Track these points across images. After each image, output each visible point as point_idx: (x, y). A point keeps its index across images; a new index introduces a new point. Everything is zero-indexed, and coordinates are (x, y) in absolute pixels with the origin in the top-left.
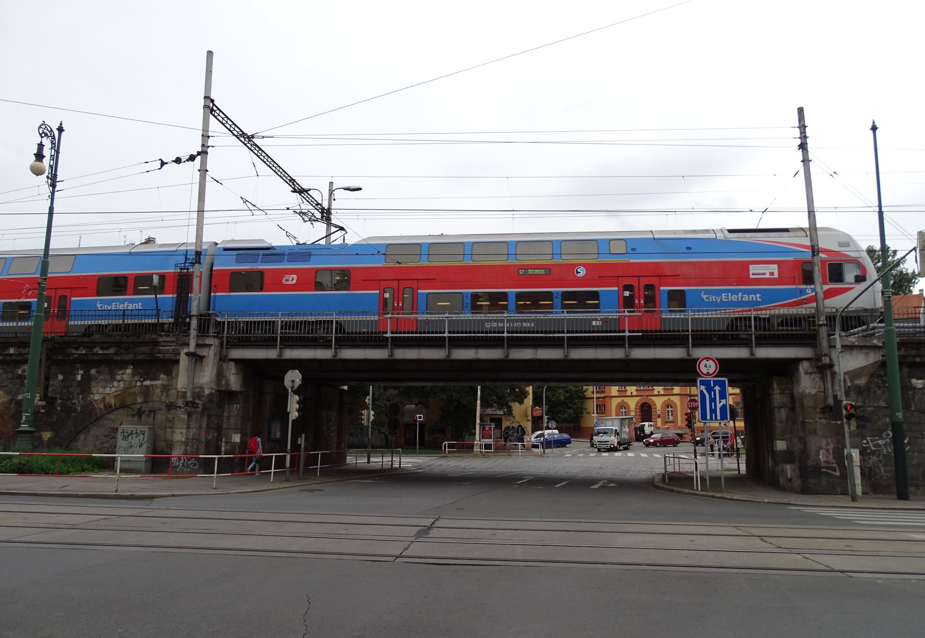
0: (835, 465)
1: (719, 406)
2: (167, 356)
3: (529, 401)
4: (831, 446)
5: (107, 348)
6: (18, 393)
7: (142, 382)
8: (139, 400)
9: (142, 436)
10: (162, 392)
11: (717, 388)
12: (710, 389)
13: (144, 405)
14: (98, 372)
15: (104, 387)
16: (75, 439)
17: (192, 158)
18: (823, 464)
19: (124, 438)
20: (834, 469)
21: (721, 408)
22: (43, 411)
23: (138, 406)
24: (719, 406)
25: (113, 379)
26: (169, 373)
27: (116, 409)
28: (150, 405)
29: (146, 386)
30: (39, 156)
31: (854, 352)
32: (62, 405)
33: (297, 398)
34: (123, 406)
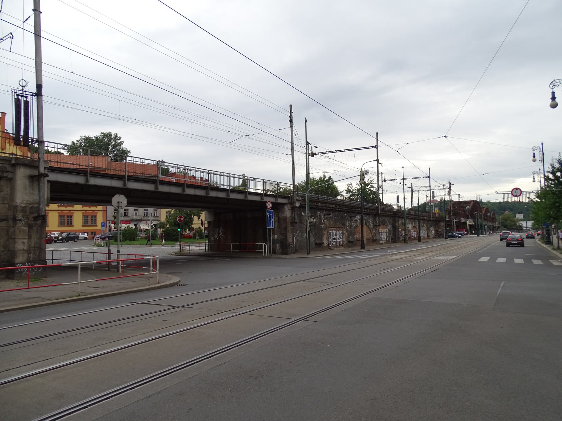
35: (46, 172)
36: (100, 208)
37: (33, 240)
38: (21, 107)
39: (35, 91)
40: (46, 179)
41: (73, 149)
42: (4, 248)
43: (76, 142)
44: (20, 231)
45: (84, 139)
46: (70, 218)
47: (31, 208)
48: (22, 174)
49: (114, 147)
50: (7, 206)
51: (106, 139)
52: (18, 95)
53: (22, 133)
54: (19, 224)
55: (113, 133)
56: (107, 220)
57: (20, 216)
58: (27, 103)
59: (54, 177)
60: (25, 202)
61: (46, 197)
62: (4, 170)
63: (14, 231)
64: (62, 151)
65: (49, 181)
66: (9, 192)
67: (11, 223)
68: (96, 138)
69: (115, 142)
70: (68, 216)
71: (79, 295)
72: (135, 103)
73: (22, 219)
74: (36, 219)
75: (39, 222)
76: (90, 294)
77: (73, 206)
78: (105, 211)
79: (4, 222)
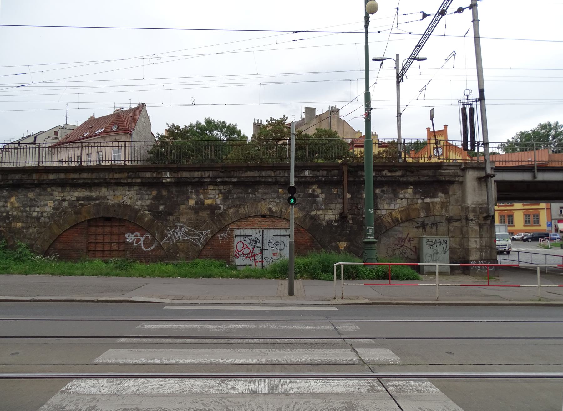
2: (448, 178)
3: (319, 213)
5: (395, 171)
6: (311, 209)
7: (423, 199)
8: (422, 214)
9: (445, 245)
10: (442, 208)
13: (426, 219)
14: (382, 191)
15: (389, 204)
19: (429, 246)
22: (336, 224)
23: (421, 220)
25: (396, 197)
26: (446, 192)
27: (402, 222)
28: (432, 219)
29: (427, 203)
32: (353, 219)
34: (409, 219)
35: (493, 173)
36: (543, 205)
37: (484, 239)
38: (467, 116)
39: (478, 97)
40: (493, 179)
41: (509, 147)
42: (459, 246)
43: (511, 140)
44: (472, 231)
45: (520, 135)
46: (510, 218)
47: (481, 208)
48: (471, 176)
49: (554, 137)
50: (460, 207)
51: (544, 131)
52: (464, 105)
53: (469, 139)
54: (471, 224)
55: (553, 122)
56: (552, 220)
57: (471, 216)
58: (471, 110)
59: (500, 176)
60: (475, 203)
61: (493, 197)
62: (456, 175)
63: (468, 230)
64: (497, 151)
65: (495, 181)
66: (461, 195)
67: (464, 222)
68: (533, 132)
69: (556, 132)
70: (509, 216)
71: (540, 300)
72: (165, 87)
73: (474, 219)
74: (485, 218)
75: (489, 222)
76: (551, 300)
77: (513, 206)
78: (549, 209)
79: (459, 222)
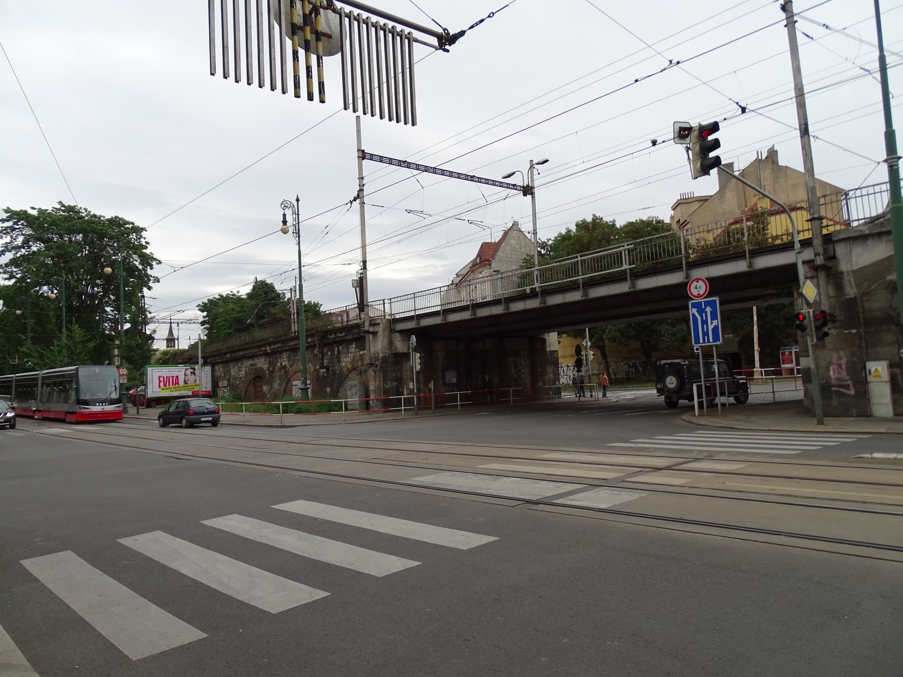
0: (850, 382)
1: (711, 327)
4: (844, 360)
11: (708, 309)
12: (701, 311)
16: (338, 391)
17: (355, 199)
18: (833, 382)
20: (847, 387)
21: (713, 330)
24: (711, 327)
30: (285, 222)
31: (870, 242)
33: (418, 355)
34: (354, 369)
